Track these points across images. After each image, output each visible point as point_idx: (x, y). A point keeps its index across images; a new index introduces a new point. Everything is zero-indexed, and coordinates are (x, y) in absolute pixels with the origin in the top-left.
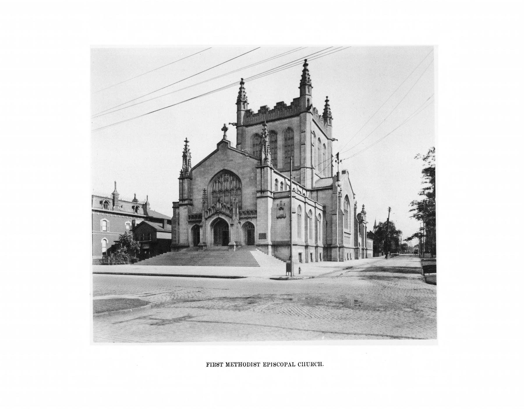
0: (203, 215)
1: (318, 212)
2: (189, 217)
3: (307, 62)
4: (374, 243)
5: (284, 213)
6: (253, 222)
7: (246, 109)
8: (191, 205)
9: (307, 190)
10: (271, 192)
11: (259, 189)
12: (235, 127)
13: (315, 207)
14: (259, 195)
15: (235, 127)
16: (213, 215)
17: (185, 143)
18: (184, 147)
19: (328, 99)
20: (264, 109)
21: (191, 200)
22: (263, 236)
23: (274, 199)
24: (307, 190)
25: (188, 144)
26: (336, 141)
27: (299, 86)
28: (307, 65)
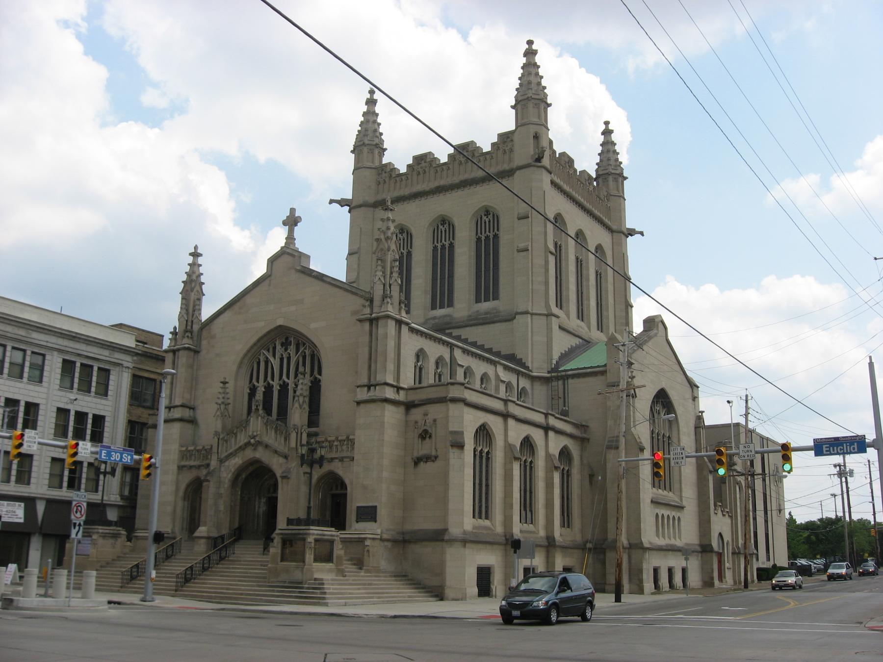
0: (215, 450)
1: (556, 444)
2: (185, 455)
3: (534, 47)
4: (12, 563)
5: (424, 450)
6: (338, 468)
7: (377, 164)
8: (193, 421)
9: (533, 379)
10: (398, 389)
11: (365, 381)
12: (347, 208)
13: (547, 429)
14: (363, 394)
15: (347, 208)
16: (242, 448)
17: (190, 259)
18: (188, 269)
19: (611, 127)
20: (423, 162)
21: (192, 408)
22: (368, 514)
23: (409, 406)
24: (533, 379)
25: (200, 260)
26: (637, 236)
27: (513, 103)
28: (535, 53)
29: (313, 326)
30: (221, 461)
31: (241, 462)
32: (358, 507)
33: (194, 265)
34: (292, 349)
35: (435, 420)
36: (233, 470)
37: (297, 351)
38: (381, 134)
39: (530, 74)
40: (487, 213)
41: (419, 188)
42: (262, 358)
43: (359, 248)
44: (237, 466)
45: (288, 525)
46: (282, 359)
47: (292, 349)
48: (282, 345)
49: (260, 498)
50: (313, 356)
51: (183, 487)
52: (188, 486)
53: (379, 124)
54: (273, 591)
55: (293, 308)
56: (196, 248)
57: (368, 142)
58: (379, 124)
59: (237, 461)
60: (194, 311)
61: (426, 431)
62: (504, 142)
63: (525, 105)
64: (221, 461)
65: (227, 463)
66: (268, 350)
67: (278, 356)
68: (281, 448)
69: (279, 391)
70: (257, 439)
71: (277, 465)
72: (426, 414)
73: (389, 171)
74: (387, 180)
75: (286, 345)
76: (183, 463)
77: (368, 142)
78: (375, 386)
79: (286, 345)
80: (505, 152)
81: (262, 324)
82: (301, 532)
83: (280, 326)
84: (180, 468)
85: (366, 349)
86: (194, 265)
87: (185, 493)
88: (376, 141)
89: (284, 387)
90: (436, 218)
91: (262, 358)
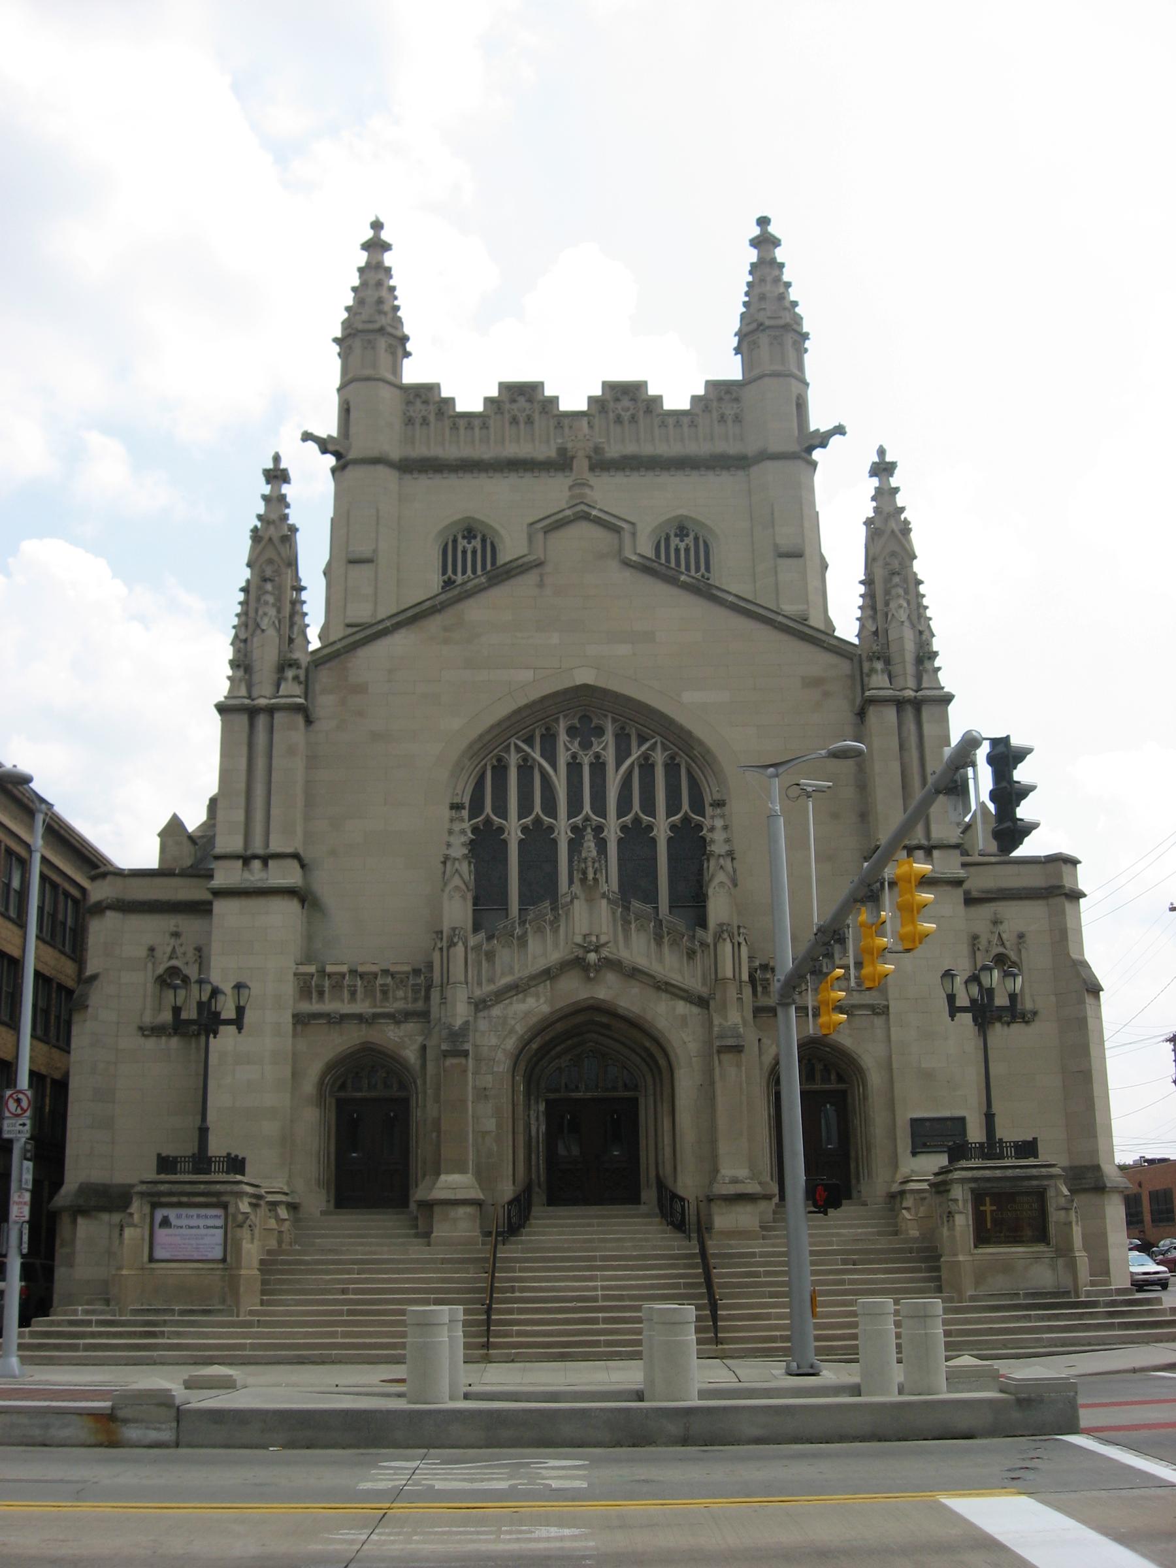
3: (771, 229)
12: (330, 460)
16: (548, 975)
29: (688, 697)
30: (480, 1005)
31: (545, 1009)
32: (914, 1122)
33: (885, 495)
34: (606, 746)
35: (1021, 936)
36: (520, 1029)
37: (622, 754)
38: (795, 304)
39: (762, 280)
40: (682, 532)
41: (513, 450)
42: (513, 760)
43: (375, 551)
44: (533, 1020)
45: (159, 1173)
46: (574, 767)
47: (606, 746)
48: (572, 731)
49: (537, 1103)
50: (672, 768)
51: (314, 1071)
52: (330, 1067)
53: (788, 285)
54: (1028, 1318)
55: (623, 649)
56: (881, 452)
57: (372, 330)
58: (788, 285)
59: (536, 1006)
60: (887, 604)
61: (173, 971)
62: (720, 399)
63: (775, 338)
64: (480, 1005)
65: (496, 1011)
66: (529, 741)
67: (563, 759)
68: (690, 978)
69: (521, 842)
70: (605, 953)
71: (672, 1021)
72: (996, 922)
73: (427, 402)
74: (432, 418)
75: (585, 732)
76: (306, 1007)
77: (372, 330)
78: (265, 859)
79: (585, 732)
80: (722, 419)
81: (528, 675)
82: (1034, 1171)
83: (586, 687)
84: (301, 1020)
85: (896, 767)
86: (885, 495)
87: (321, 1083)
88: (787, 319)
89: (538, 839)
90: (669, 521)
91: (513, 760)
